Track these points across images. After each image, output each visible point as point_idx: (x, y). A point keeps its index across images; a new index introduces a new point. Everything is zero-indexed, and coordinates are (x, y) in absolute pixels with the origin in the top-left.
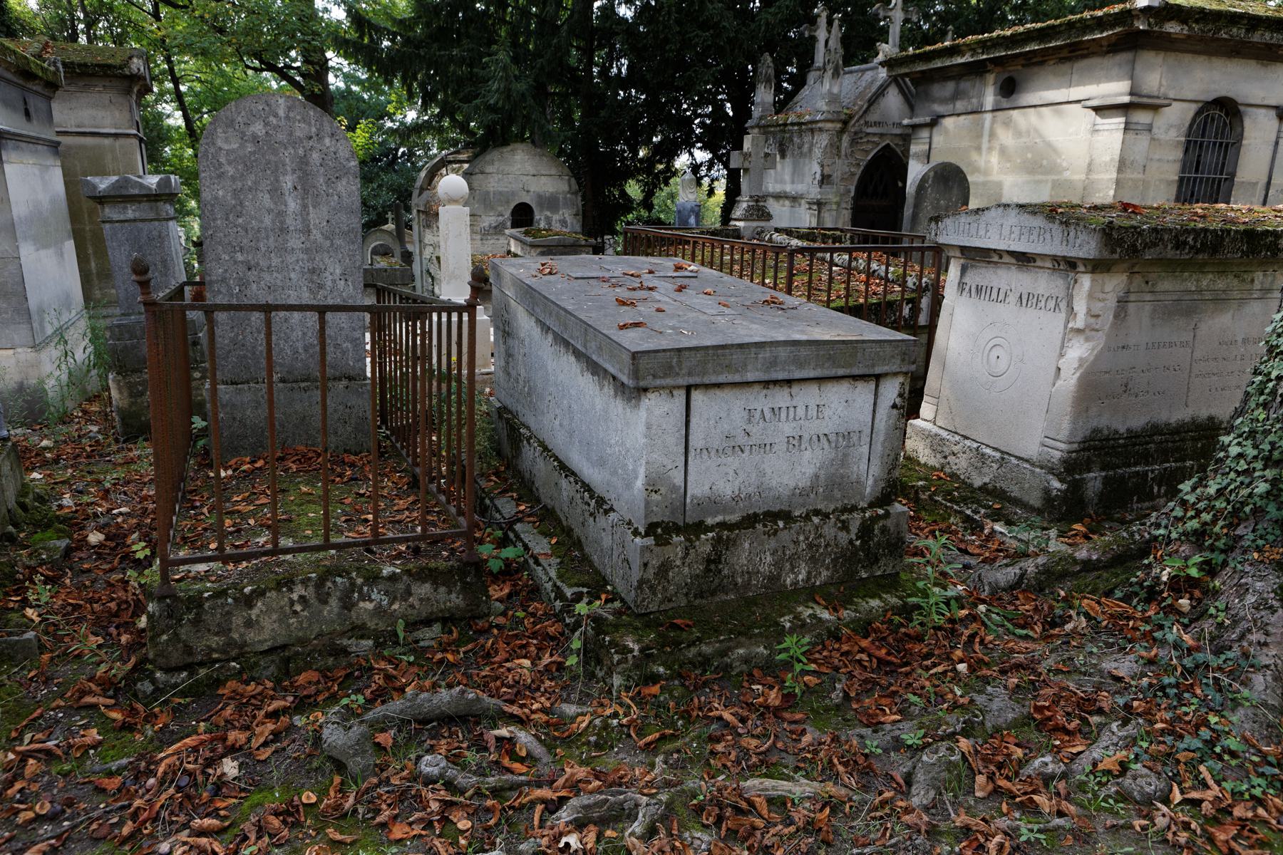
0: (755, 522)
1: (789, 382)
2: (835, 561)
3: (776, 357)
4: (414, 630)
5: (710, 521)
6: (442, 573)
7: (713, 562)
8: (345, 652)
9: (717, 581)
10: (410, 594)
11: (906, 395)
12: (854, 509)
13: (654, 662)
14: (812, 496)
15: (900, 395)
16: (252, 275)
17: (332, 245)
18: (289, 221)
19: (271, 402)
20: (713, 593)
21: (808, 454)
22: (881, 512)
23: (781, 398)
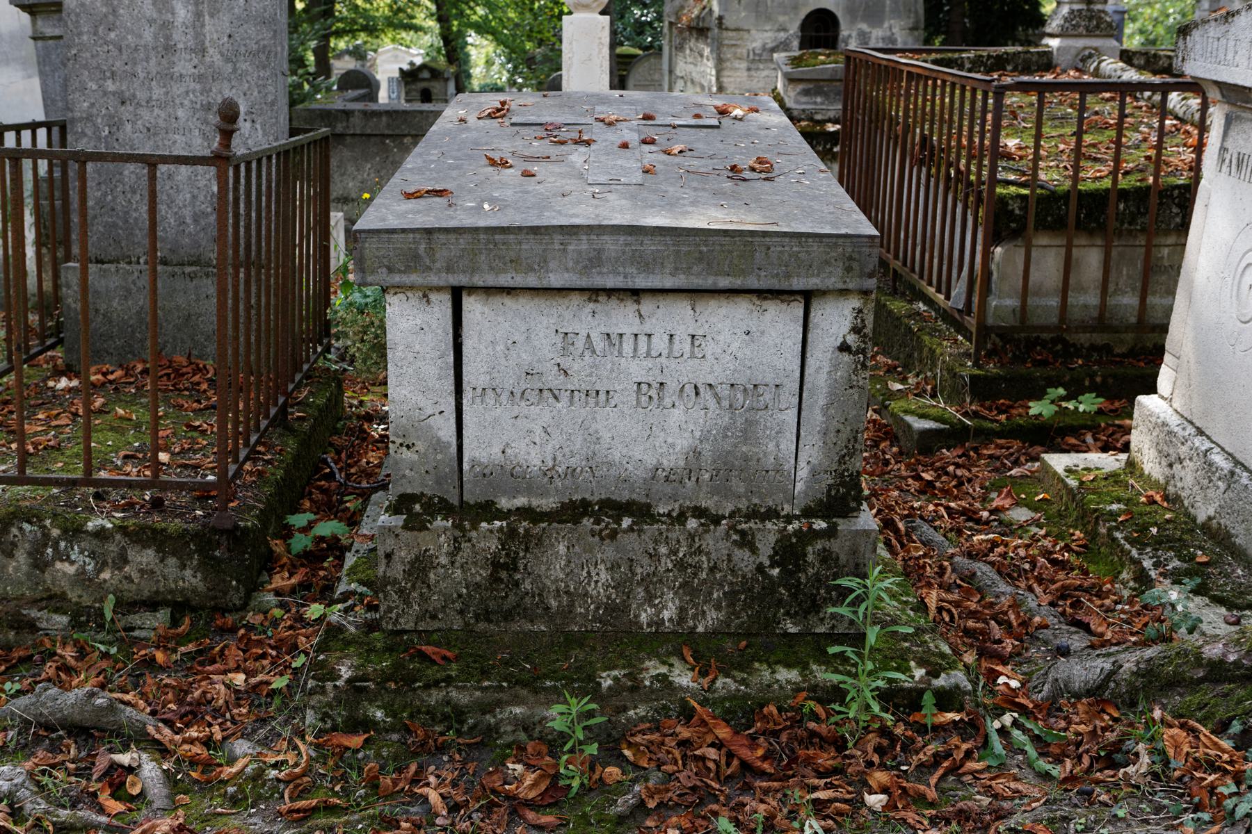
0: (585, 514)
1: (636, 294)
2: (731, 596)
3: (599, 251)
4: (129, 612)
5: (504, 503)
6: (170, 537)
7: (503, 568)
8: (32, 626)
9: (512, 599)
10: (126, 562)
11: (868, 330)
12: (772, 514)
13: (371, 702)
14: (689, 484)
15: (855, 330)
16: (126, 112)
17: (235, 70)
18: (177, 36)
19: (154, 290)
20: (508, 616)
21: (677, 415)
22: (820, 525)
23: (622, 318)
